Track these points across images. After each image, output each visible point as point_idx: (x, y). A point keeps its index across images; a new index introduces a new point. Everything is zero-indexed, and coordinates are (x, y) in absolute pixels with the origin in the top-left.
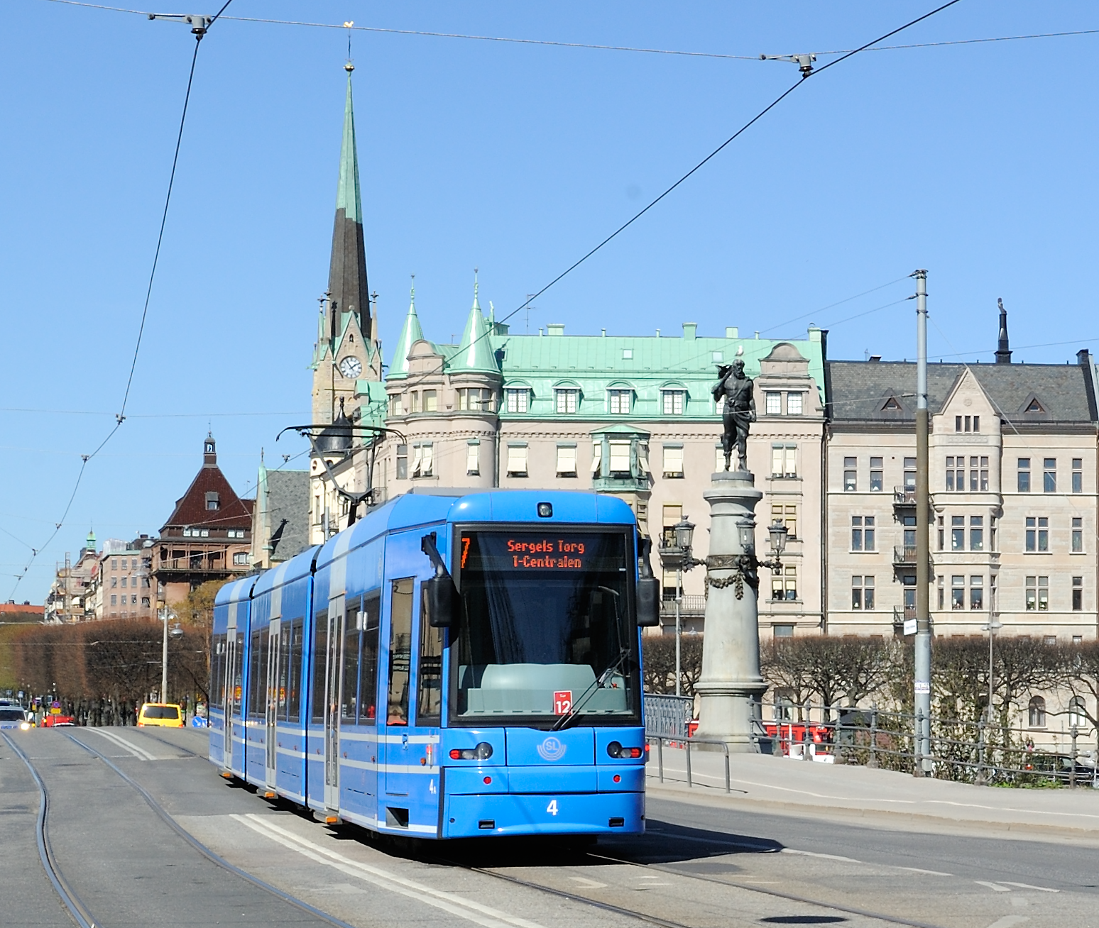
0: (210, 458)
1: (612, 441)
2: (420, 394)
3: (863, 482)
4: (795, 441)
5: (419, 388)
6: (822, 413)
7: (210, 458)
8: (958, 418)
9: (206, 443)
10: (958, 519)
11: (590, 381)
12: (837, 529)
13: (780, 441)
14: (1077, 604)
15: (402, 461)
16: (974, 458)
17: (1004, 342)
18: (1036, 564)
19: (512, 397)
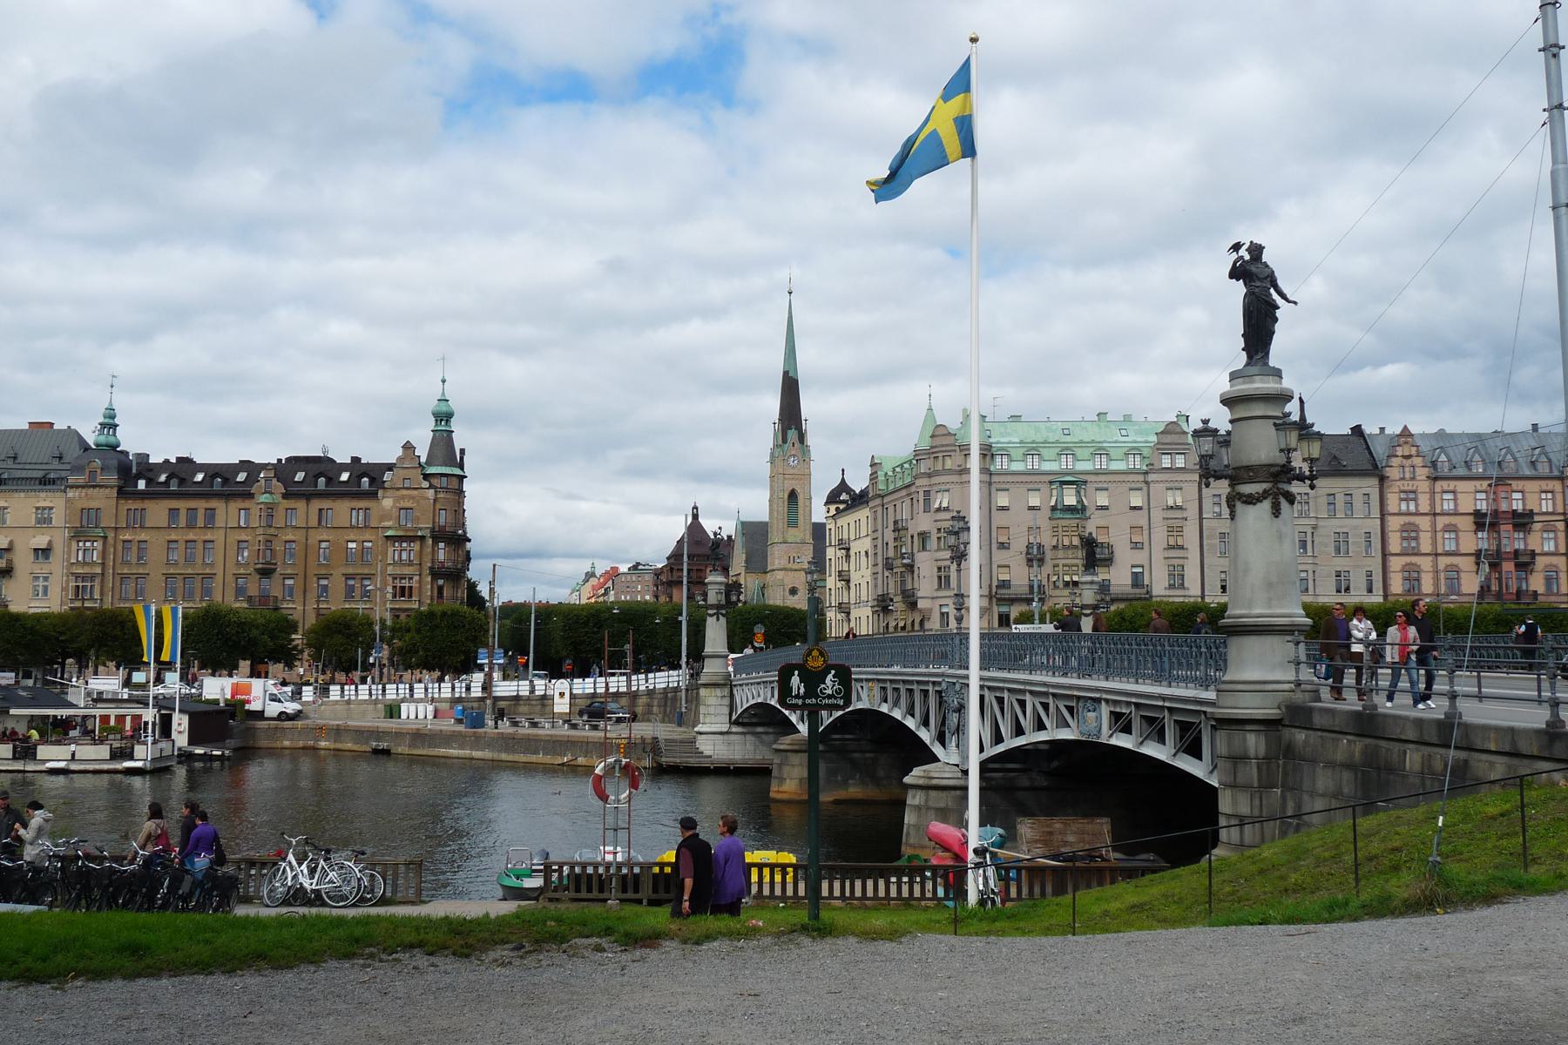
0: (695, 517)
1: (1064, 486)
2: (941, 458)
4: (1181, 485)
5: (940, 455)
6: (1198, 467)
7: (695, 517)
9: (693, 509)
11: (1047, 449)
12: (1209, 541)
13: (1172, 485)
14: (1370, 590)
15: (927, 502)
18: (1341, 563)
19: (998, 459)
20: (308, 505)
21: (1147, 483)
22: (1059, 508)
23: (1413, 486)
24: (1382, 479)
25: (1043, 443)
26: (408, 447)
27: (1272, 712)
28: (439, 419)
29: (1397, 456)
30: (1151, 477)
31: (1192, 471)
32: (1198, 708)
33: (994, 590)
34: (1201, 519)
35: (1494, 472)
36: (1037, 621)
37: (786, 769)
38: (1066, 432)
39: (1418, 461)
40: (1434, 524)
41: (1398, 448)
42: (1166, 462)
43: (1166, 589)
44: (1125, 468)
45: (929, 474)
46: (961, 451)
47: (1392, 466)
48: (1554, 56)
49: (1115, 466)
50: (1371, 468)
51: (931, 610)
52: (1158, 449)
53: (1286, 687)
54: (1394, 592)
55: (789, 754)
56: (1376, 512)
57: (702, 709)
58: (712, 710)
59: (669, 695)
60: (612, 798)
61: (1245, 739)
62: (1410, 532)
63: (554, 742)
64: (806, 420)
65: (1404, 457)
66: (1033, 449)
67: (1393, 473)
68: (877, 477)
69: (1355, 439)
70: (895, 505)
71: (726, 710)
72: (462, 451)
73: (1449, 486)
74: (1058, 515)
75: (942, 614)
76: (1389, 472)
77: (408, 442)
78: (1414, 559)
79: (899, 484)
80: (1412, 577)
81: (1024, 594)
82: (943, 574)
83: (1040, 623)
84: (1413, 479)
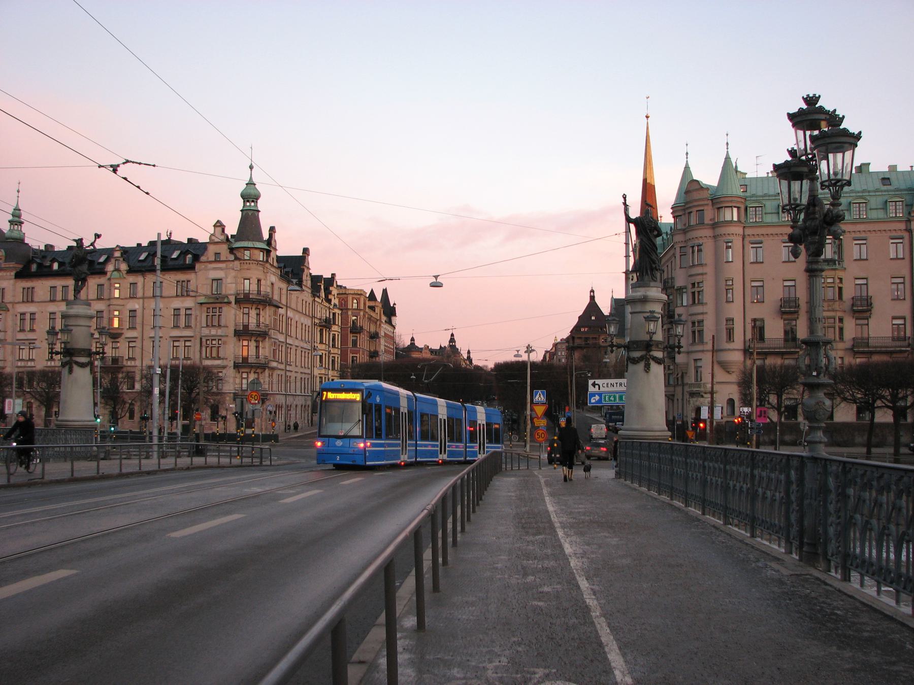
9: (591, 292)
20: (144, 279)
25: (875, 191)
26: (219, 225)
28: (246, 200)
33: (747, 344)
45: (684, 230)
46: (713, 204)
64: (661, 217)
72: (272, 230)
77: (218, 221)
81: (777, 348)
82: (696, 329)
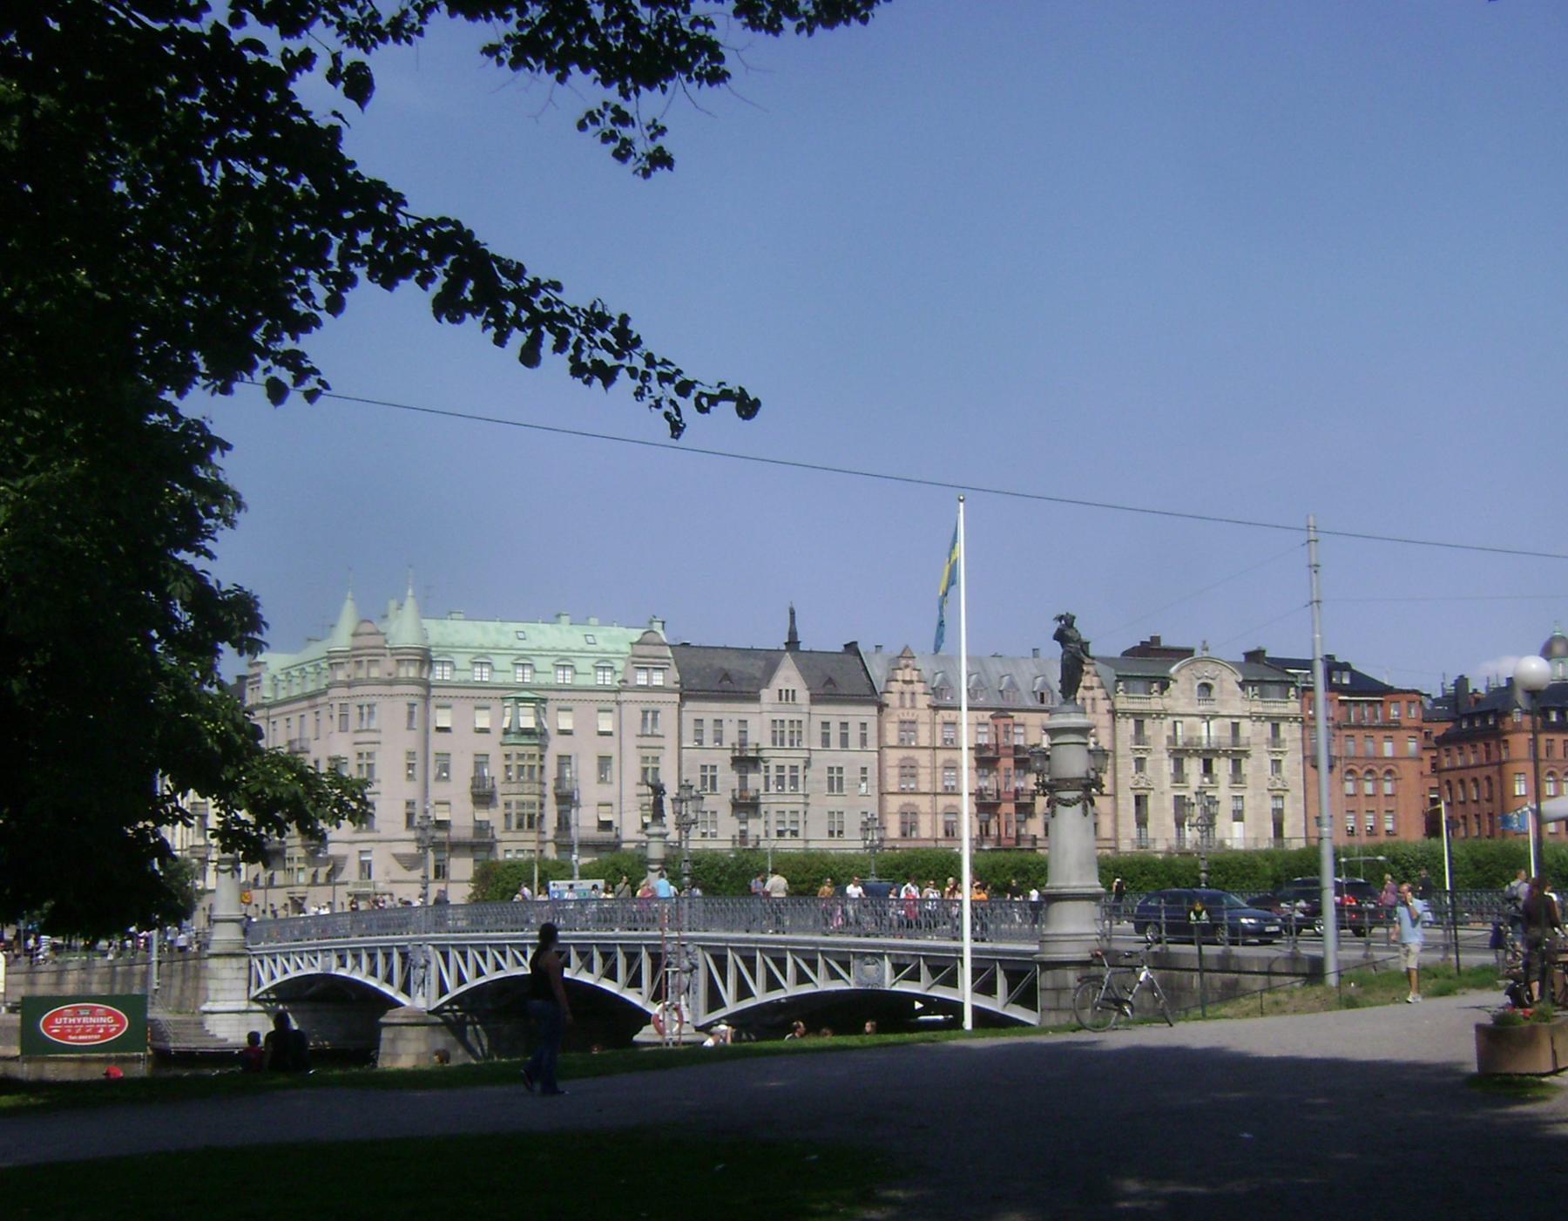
3: (708, 741)
6: (678, 686)
8: (780, 691)
10: (780, 768)
16: (792, 722)
17: (793, 634)
19: (438, 668)
21: (618, 703)
22: (513, 730)
23: (913, 715)
24: (882, 707)
25: (493, 648)
27: (1086, 956)
29: (897, 681)
30: (624, 696)
31: (672, 691)
32: (994, 957)
34: (680, 748)
35: (996, 702)
36: (577, 877)
37: (401, 1045)
38: (521, 635)
39: (919, 687)
40: (934, 760)
41: (898, 671)
42: (642, 679)
43: (638, 832)
44: (593, 684)
47: (891, 692)
48: (1316, 572)
49: (581, 681)
50: (869, 693)
51: (345, 858)
52: (633, 663)
53: (1094, 937)
54: (891, 837)
55: (404, 1027)
56: (872, 744)
57: (212, 984)
58: (226, 985)
59: (119, 969)
60: (668, 1031)
61: (1066, 975)
62: (908, 770)
63: (7, 1028)
65: (905, 682)
66: (482, 655)
67: (892, 699)
68: (259, 681)
69: (850, 658)
70: (288, 720)
71: (244, 985)
73: (950, 716)
74: (512, 739)
75: (362, 863)
76: (888, 698)
78: (911, 799)
79: (296, 692)
80: (909, 824)
83: (581, 879)
84: (913, 707)
